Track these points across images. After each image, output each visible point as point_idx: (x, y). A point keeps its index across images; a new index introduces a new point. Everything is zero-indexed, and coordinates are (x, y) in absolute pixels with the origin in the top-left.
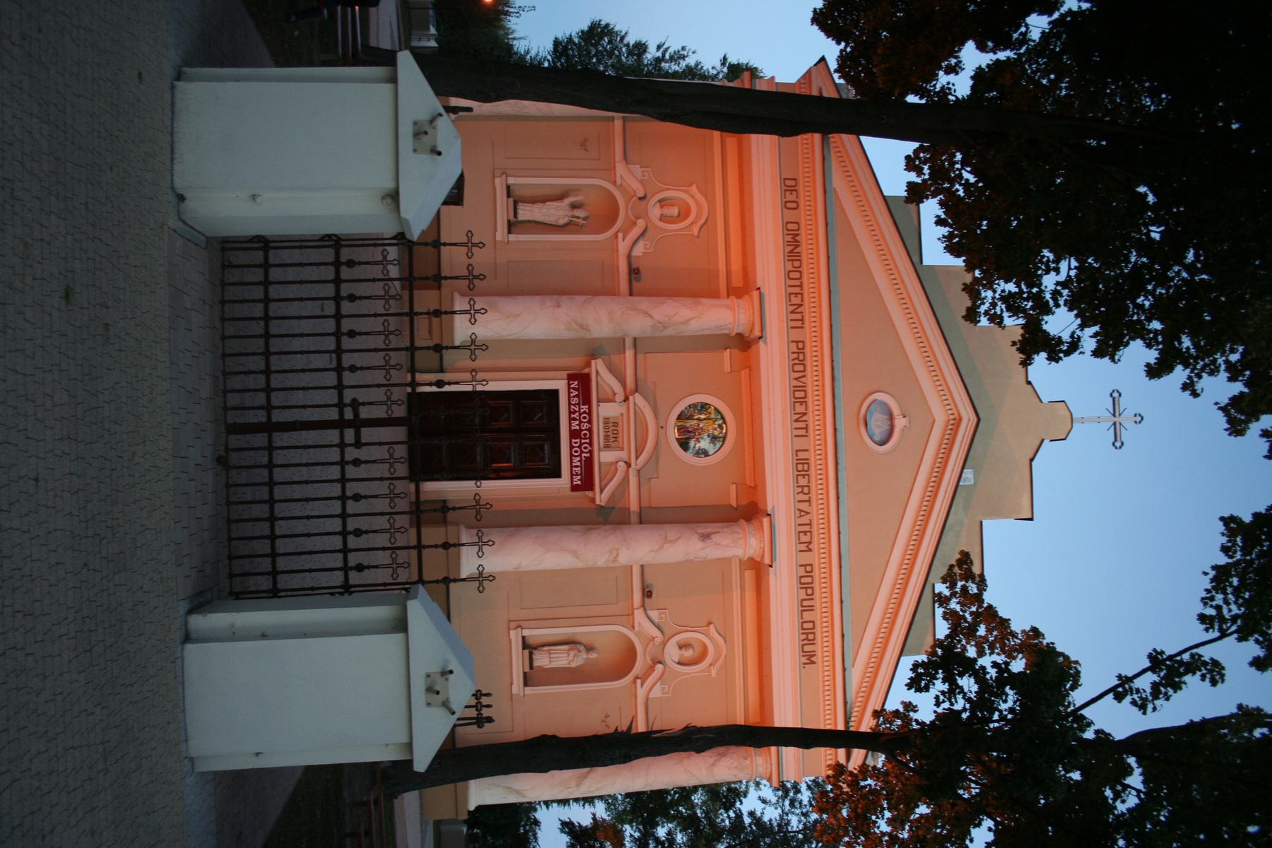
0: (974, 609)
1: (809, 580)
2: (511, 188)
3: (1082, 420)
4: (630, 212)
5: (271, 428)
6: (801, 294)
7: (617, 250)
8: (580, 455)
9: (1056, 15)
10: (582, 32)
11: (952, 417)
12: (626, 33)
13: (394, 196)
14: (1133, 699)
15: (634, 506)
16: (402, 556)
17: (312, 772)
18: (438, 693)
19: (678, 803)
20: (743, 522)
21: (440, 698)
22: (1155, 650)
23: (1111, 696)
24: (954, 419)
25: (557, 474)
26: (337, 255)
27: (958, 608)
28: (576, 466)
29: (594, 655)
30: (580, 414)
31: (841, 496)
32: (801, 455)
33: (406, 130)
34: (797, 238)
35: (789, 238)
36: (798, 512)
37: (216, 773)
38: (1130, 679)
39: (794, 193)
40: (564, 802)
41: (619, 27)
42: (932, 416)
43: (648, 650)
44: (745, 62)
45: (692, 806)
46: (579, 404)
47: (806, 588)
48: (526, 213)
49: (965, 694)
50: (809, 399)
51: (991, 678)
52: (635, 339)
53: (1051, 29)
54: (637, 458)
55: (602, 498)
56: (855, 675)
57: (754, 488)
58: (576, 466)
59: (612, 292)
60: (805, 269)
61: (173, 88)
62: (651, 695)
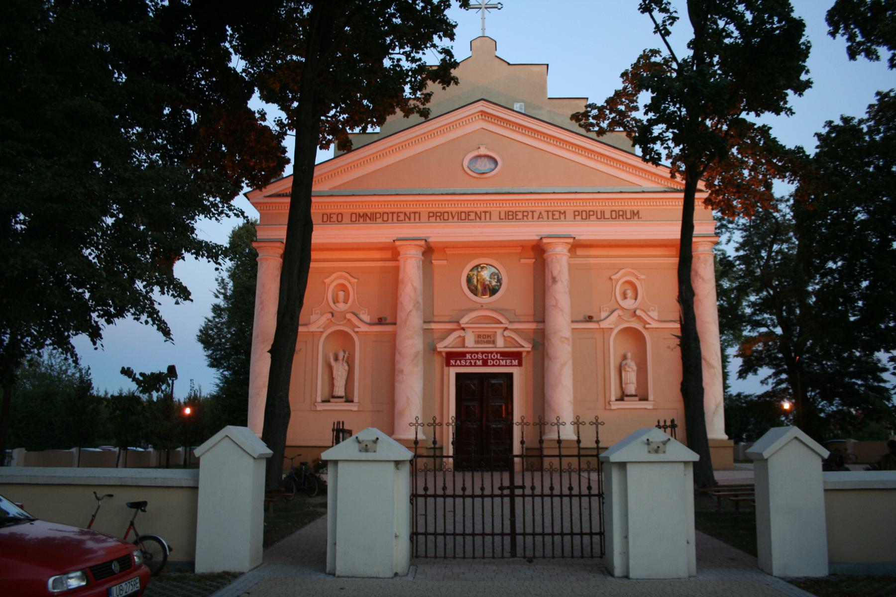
0: (607, 112)
1: (584, 213)
2: (324, 399)
3: (483, 29)
4: (341, 323)
5: (513, 534)
6: (398, 213)
7: (366, 332)
8: (499, 360)
9: (231, 50)
10: (204, 348)
11: (480, 117)
12: (206, 318)
13: (397, 463)
14: (669, 24)
15: (533, 326)
16: (584, 466)
17: (698, 526)
18: (658, 447)
19: (729, 298)
20: (545, 256)
21: (661, 445)
22: (639, 9)
23: (667, 38)
24: (482, 115)
25: (510, 376)
26: (421, 496)
27: (607, 122)
28: (506, 363)
29: (629, 355)
30: (472, 359)
31: (530, 191)
32: (503, 216)
33: (364, 456)
34: (361, 214)
35: (361, 220)
36: (540, 219)
37: (697, 568)
38: (657, 26)
39: (332, 216)
40: (725, 376)
41: (202, 323)
42: (479, 129)
43: (626, 319)
44: (229, 239)
45: (731, 290)
46: (466, 360)
47: (589, 215)
48: (340, 390)
49: (663, 132)
50: (466, 210)
51: (654, 116)
52: (425, 322)
53: (240, 53)
54: (501, 323)
55: (527, 347)
56: (647, 185)
57: (523, 247)
58: (506, 363)
59: (394, 336)
60: (382, 211)
61: (338, 577)
62: (656, 318)
